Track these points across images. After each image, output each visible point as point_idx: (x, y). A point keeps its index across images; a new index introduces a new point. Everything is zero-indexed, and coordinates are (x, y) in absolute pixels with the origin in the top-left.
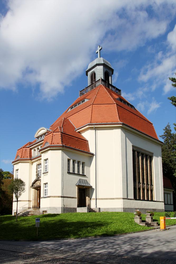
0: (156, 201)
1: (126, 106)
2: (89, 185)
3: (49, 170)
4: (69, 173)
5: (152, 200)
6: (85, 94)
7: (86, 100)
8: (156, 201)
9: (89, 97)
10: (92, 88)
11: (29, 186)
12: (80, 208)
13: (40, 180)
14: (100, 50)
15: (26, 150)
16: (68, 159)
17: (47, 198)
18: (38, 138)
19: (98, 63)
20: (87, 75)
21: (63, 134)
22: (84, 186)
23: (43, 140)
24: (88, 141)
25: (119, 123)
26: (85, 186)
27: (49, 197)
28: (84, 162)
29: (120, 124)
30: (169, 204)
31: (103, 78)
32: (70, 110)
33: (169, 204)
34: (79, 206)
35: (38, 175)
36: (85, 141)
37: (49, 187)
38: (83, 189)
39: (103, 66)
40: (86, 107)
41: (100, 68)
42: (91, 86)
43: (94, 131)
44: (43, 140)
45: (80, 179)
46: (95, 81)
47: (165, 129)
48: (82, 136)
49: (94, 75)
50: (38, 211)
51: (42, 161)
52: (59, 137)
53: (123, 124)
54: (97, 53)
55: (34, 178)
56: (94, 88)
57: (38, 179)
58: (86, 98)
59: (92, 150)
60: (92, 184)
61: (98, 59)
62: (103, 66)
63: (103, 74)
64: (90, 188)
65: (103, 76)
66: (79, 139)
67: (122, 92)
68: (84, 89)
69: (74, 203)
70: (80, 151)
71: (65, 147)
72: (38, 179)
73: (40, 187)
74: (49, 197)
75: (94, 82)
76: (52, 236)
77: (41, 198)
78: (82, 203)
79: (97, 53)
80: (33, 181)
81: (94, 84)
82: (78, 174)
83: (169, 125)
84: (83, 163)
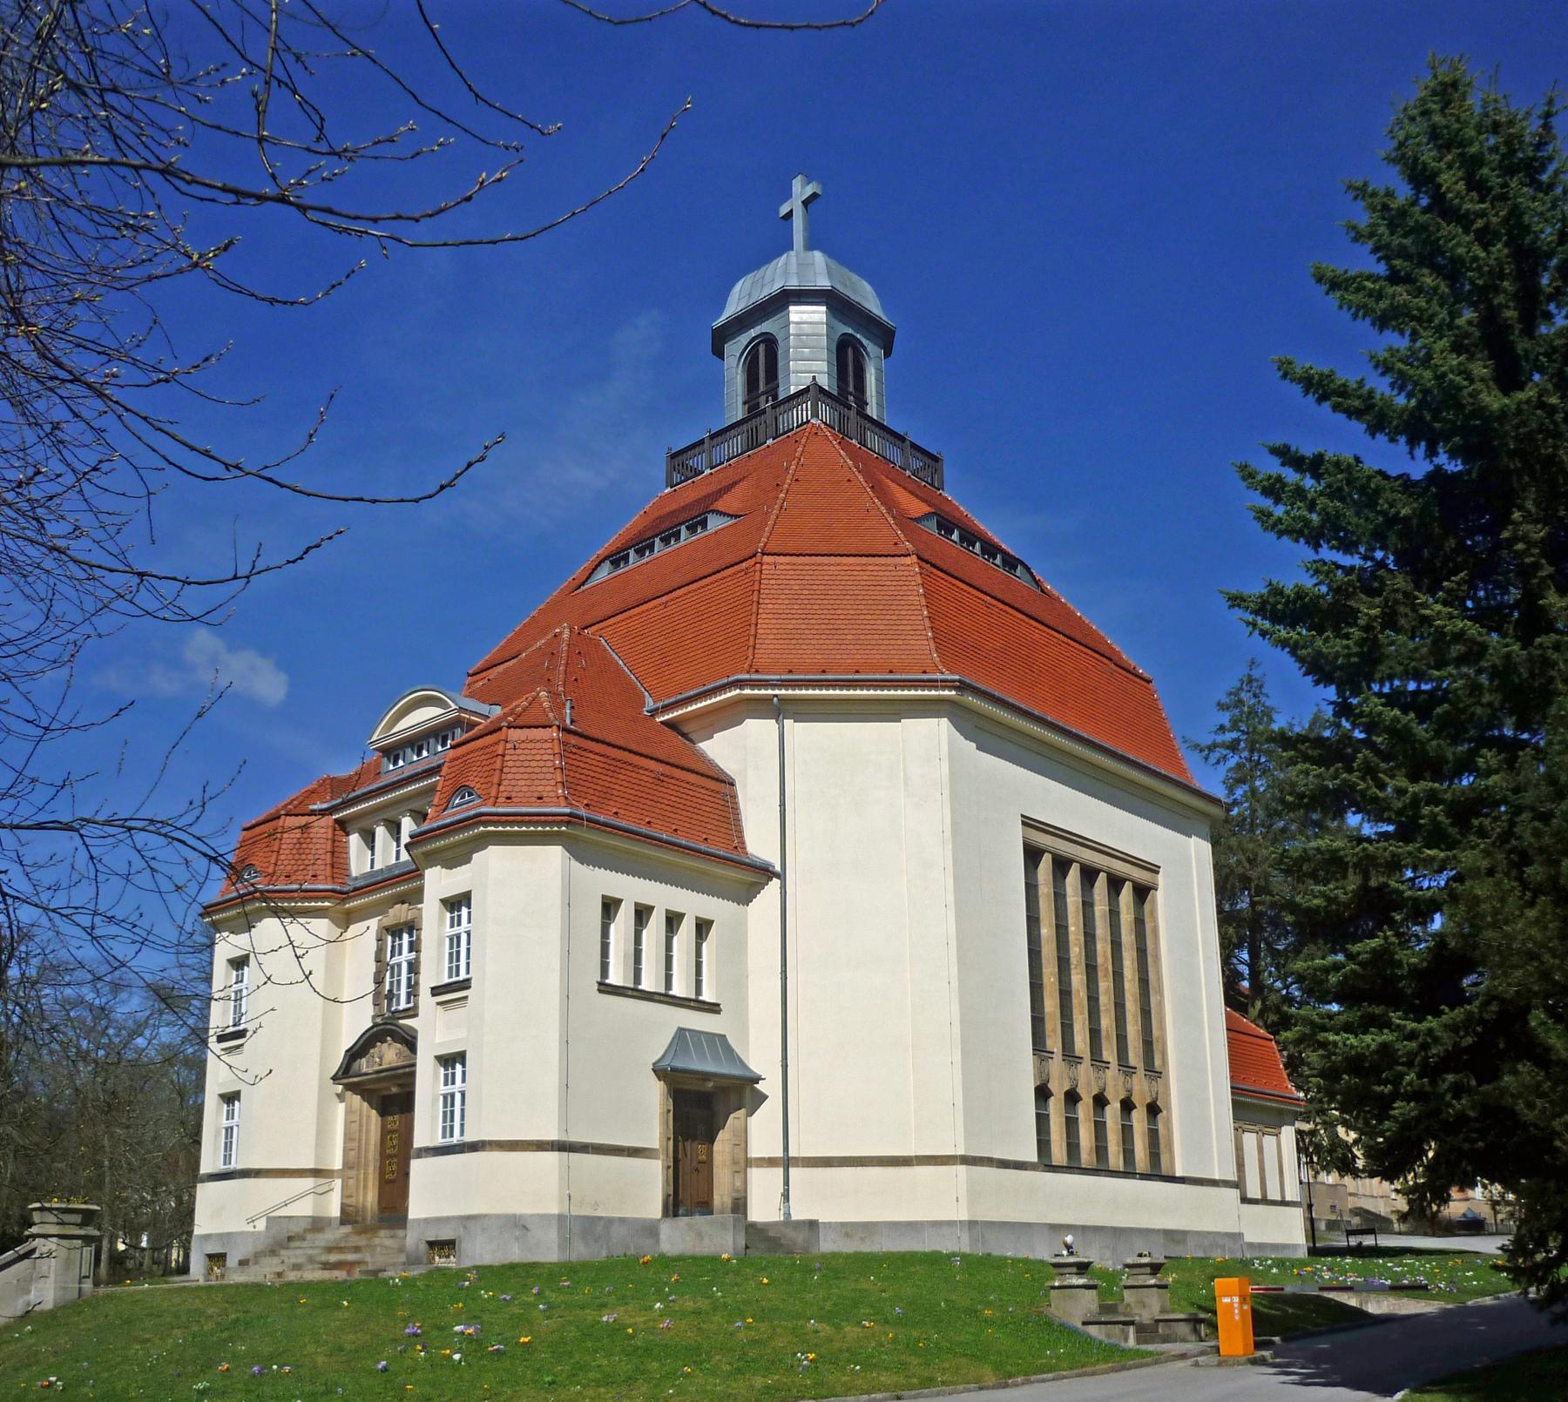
0: (1182, 1180)
1: (973, 561)
2: (748, 1074)
3: (485, 970)
4: (605, 988)
5: (1157, 1173)
6: (708, 472)
7: (715, 523)
8: (1182, 1180)
9: (728, 502)
10: (753, 443)
11: (322, 1073)
12: (683, 1221)
13: (409, 1042)
14: (806, 203)
15: (305, 828)
16: (636, 904)
17: (462, 1152)
18: (391, 752)
19: (793, 283)
20: (719, 352)
21: (573, 740)
22: (706, 1076)
23: (435, 771)
24: (732, 784)
25: (939, 676)
26: (715, 1075)
27: (474, 1147)
28: (681, 910)
29: (945, 684)
30: (1274, 1203)
31: (823, 381)
32: (604, 573)
33: (1274, 1203)
34: (674, 1207)
35: (383, 996)
36: (713, 785)
37: (477, 1077)
38: (698, 1093)
39: (824, 308)
40: (716, 566)
41: (805, 317)
42: (745, 427)
43: (770, 725)
44: (435, 771)
45: (681, 1031)
46: (775, 397)
47: (1225, 700)
48: (702, 757)
49: (765, 362)
50: (388, 1242)
51: (430, 912)
52: (546, 757)
53: (962, 687)
54: (790, 214)
55: (357, 1020)
56: (770, 442)
57: (390, 1029)
58: (719, 505)
59: (760, 843)
60: (760, 1058)
61: (794, 260)
62: (824, 308)
63: (825, 355)
64: (748, 1090)
65: (823, 366)
66: (677, 773)
67: (948, 472)
68: (702, 442)
69: (642, 1189)
70: (680, 846)
71: (589, 820)
72: (390, 1029)
73: (405, 1078)
74: (474, 1147)
75: (765, 403)
76: (1499, 299)
77: (419, 1157)
78: (688, 1192)
79: (790, 214)
80: (348, 1039)
81: (769, 416)
82: (667, 999)
83: (1256, 674)
84: (703, 927)
